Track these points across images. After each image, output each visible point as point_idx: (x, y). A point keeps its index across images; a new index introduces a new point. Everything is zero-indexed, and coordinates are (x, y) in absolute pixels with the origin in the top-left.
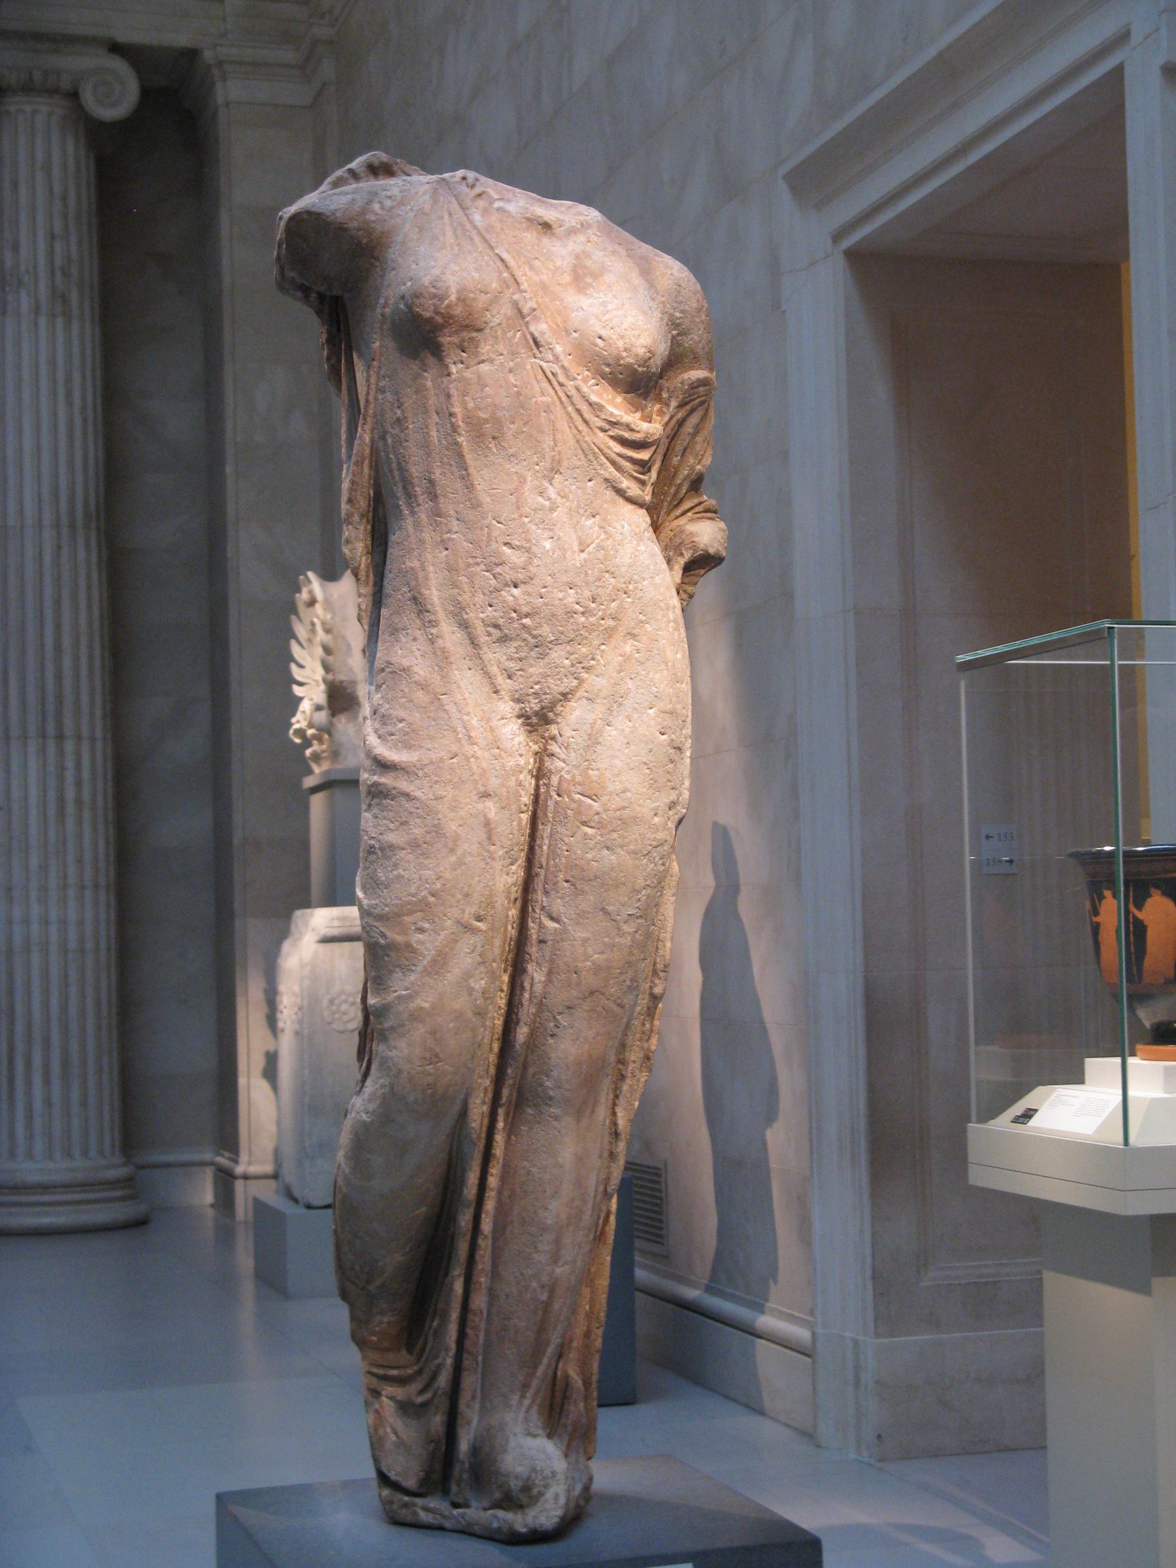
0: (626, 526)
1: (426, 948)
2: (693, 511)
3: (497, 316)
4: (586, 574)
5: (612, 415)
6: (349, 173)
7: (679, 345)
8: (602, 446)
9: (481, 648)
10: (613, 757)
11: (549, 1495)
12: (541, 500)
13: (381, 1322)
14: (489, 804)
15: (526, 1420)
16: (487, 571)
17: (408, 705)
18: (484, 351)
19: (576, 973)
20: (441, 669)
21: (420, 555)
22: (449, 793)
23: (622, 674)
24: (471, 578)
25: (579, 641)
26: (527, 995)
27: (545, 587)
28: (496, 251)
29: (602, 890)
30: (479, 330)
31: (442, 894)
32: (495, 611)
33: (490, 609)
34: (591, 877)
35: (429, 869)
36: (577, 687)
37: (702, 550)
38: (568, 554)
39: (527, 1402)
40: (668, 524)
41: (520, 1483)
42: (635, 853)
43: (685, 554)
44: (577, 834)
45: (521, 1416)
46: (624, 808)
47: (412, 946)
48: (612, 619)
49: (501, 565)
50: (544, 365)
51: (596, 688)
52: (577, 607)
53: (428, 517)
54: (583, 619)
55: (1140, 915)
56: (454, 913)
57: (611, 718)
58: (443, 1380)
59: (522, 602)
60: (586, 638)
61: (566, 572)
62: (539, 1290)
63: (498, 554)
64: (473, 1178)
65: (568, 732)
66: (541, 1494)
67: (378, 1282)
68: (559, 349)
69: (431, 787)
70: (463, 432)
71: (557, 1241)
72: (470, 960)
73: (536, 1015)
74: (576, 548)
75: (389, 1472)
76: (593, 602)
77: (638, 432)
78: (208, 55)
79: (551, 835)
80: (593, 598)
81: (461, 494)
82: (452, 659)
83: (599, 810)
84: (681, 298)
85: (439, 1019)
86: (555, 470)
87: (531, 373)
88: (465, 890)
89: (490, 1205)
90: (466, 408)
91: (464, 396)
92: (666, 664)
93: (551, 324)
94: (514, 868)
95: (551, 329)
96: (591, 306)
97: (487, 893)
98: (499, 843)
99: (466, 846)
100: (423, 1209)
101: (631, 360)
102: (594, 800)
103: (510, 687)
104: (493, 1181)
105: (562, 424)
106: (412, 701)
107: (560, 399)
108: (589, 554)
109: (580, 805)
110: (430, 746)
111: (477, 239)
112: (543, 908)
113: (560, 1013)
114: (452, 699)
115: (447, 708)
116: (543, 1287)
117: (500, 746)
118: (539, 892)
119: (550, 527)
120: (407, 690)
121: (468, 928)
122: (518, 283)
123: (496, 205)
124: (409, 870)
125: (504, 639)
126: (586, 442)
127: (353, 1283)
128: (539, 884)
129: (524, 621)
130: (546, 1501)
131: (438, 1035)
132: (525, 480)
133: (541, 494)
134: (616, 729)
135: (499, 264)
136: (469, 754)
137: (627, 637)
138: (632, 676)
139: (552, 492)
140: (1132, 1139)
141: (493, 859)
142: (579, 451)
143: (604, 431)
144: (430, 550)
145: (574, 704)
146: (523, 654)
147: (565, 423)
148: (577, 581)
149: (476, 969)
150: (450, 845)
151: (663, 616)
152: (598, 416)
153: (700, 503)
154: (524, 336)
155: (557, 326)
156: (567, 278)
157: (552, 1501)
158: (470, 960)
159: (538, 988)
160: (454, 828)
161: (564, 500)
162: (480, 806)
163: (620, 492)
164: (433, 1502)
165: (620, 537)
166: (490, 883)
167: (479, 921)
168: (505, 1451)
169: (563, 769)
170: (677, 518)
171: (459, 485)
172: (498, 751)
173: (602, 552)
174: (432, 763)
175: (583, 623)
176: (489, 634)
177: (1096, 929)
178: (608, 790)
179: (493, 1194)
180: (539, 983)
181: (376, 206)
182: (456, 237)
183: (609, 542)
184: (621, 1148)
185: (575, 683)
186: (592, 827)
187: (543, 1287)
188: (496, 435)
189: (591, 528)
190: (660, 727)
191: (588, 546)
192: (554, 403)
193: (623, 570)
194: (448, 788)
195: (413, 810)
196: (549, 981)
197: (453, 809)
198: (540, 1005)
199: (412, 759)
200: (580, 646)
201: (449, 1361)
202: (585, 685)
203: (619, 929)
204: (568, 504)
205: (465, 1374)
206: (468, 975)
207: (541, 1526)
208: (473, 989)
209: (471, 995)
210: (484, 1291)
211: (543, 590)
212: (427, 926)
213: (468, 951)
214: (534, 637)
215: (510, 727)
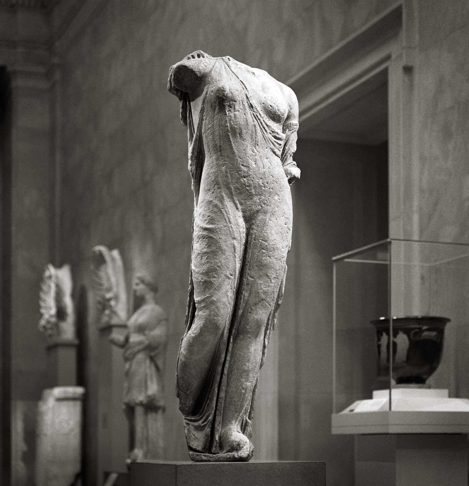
1: (216, 282)
5: (273, 129)
6: (192, 56)
8: (270, 138)
10: (271, 229)
11: (245, 448)
14: (235, 241)
15: (237, 428)
19: (258, 293)
26: (242, 300)
30: (235, 101)
31: (221, 267)
33: (237, 184)
35: (217, 259)
37: (293, 175)
46: (274, 245)
47: (211, 281)
52: (262, 185)
55: (396, 340)
58: (211, 418)
59: (246, 182)
60: (264, 194)
64: (223, 356)
70: (230, 132)
73: (245, 306)
75: (193, 446)
78: (10, 69)
79: (252, 252)
80: (267, 182)
86: (256, 144)
89: (227, 365)
102: (265, 242)
104: (228, 358)
112: (248, 274)
113: (252, 306)
115: (223, 212)
117: (239, 225)
118: (247, 270)
119: (255, 161)
125: (240, 193)
126: (266, 137)
127: (182, 391)
128: (247, 267)
129: (247, 188)
130: (244, 449)
131: (218, 309)
136: (230, 226)
140: (393, 409)
143: (270, 133)
145: (260, 214)
146: (246, 198)
148: (262, 177)
152: (269, 129)
156: (260, 89)
159: (246, 298)
162: (232, 241)
167: (231, 276)
169: (256, 233)
171: (228, 147)
172: (238, 226)
175: (264, 189)
176: (236, 191)
177: (379, 346)
178: (270, 239)
179: (228, 362)
183: (271, 167)
184: (266, 351)
186: (265, 250)
188: (240, 133)
191: (266, 167)
193: (276, 175)
196: (249, 296)
197: (225, 242)
198: (246, 303)
201: (213, 412)
205: (217, 417)
210: (224, 392)
211: (253, 179)
212: (216, 276)
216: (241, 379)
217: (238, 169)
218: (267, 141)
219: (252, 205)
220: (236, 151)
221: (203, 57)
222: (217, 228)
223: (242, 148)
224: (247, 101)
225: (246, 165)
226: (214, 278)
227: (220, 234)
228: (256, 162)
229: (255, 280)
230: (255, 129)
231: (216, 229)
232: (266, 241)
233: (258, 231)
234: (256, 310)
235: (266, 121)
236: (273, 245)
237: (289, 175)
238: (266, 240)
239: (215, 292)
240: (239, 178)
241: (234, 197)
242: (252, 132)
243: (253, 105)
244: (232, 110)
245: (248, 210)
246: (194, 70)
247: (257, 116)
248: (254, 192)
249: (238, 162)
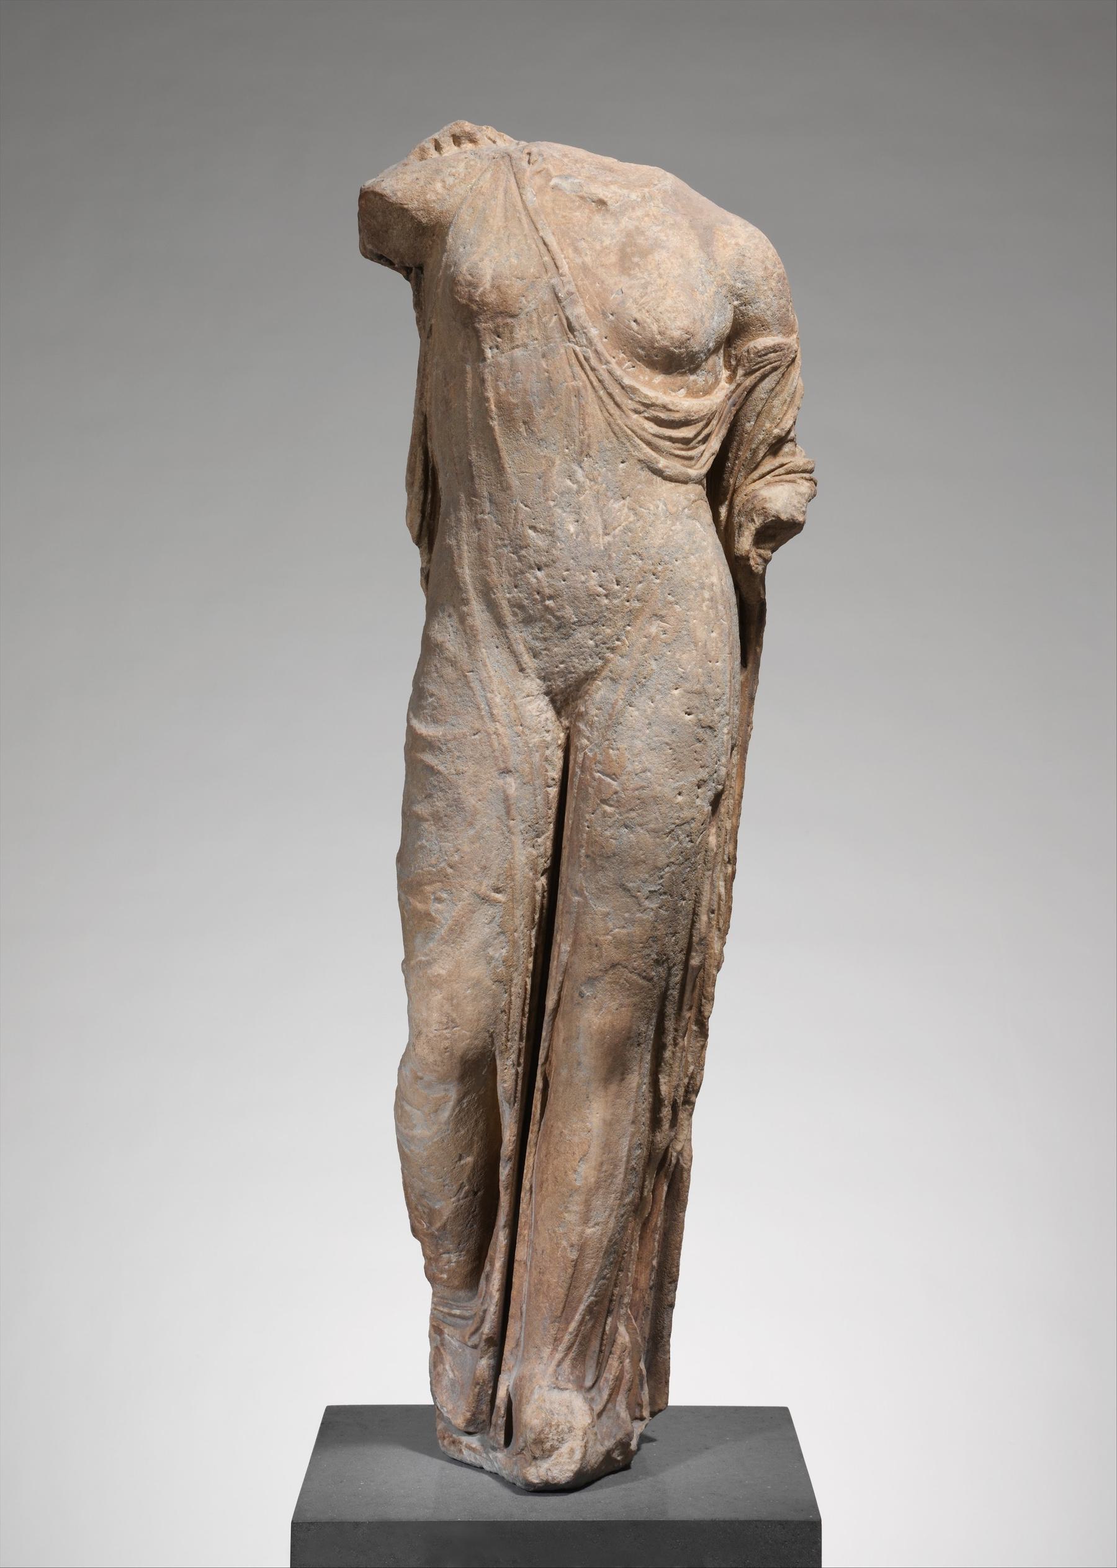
0: (661, 505)
1: (444, 918)
2: (773, 474)
3: (534, 302)
5: (646, 396)
8: (636, 428)
9: (507, 628)
10: (633, 737)
11: (565, 1449)
12: (569, 482)
13: (449, 1262)
15: (556, 1374)
16: (513, 553)
18: (518, 336)
20: (469, 646)
21: (457, 533)
22: (470, 769)
23: (646, 655)
24: (498, 558)
27: (568, 570)
28: (541, 234)
29: (621, 867)
30: (513, 316)
32: (520, 592)
34: (610, 854)
35: (448, 842)
36: (602, 667)
37: (773, 516)
38: (592, 538)
39: (558, 1356)
40: (744, 488)
41: (533, 1436)
43: (756, 519)
44: (597, 811)
45: (551, 1369)
46: (643, 788)
47: (430, 914)
48: (638, 600)
49: (526, 547)
50: (578, 349)
52: (600, 589)
54: (606, 601)
57: (633, 699)
59: (545, 584)
60: (610, 619)
61: (589, 555)
62: (569, 1249)
63: (522, 536)
65: (594, 712)
66: (554, 1449)
68: (594, 332)
69: (453, 762)
71: (587, 1203)
72: (487, 930)
80: (617, 581)
82: (480, 637)
83: (618, 789)
84: (744, 269)
85: (456, 986)
86: (584, 452)
87: (564, 357)
90: (498, 393)
91: (497, 381)
92: (696, 644)
93: (588, 306)
94: (539, 840)
95: (588, 312)
96: (630, 287)
97: (506, 866)
100: (469, 1160)
101: (666, 343)
102: (613, 779)
103: (536, 665)
105: (593, 408)
106: (442, 676)
107: (591, 383)
108: (614, 537)
110: (454, 722)
116: (572, 1246)
119: (577, 511)
120: (439, 665)
121: (485, 900)
122: (557, 267)
124: (431, 841)
125: (528, 621)
126: (618, 425)
129: (547, 602)
131: (455, 1001)
132: (554, 463)
133: (570, 477)
134: (638, 710)
135: (542, 247)
136: (492, 730)
138: (657, 657)
139: (580, 474)
141: (512, 833)
142: (612, 434)
143: (636, 411)
144: (465, 529)
145: (600, 683)
147: (597, 407)
148: (600, 564)
149: (495, 938)
150: (469, 819)
152: (631, 399)
153: (782, 465)
154: (560, 319)
155: (595, 308)
156: (613, 258)
157: (566, 1456)
158: (487, 930)
160: (474, 802)
161: (592, 483)
162: (501, 782)
163: (658, 472)
164: (474, 1441)
165: (653, 518)
166: (510, 857)
169: (587, 746)
170: (755, 481)
172: (521, 728)
173: (630, 534)
174: (455, 738)
175: (606, 605)
178: (627, 769)
180: (565, 952)
182: (506, 218)
185: (600, 663)
186: (611, 806)
187: (572, 1246)
188: (526, 419)
189: (619, 510)
190: (686, 707)
191: (614, 529)
192: (585, 387)
193: (652, 551)
195: (436, 783)
196: (573, 951)
197: (475, 784)
198: (565, 972)
200: (604, 627)
202: (610, 665)
203: (640, 905)
204: (596, 487)
206: (486, 944)
207: (553, 1478)
208: (492, 958)
211: (565, 573)
212: (444, 896)
213: (486, 921)
214: (557, 618)
215: (536, 704)
216: (566, 1215)
217: (519, 542)
219: (570, 656)
220: (515, 482)
221: (473, 141)
222: (449, 737)
223: (532, 470)
224: (558, 310)
225: (542, 526)
227: (459, 757)
228: (578, 514)
230: (580, 403)
231: (449, 741)
232: (613, 776)
233: (591, 743)
234: (595, 998)
236: (637, 790)
237: (758, 515)
238: (614, 774)
240: (522, 572)
241: (508, 631)
242: (569, 414)
243: (575, 324)
245: (558, 672)
247: (587, 359)
249: (520, 517)
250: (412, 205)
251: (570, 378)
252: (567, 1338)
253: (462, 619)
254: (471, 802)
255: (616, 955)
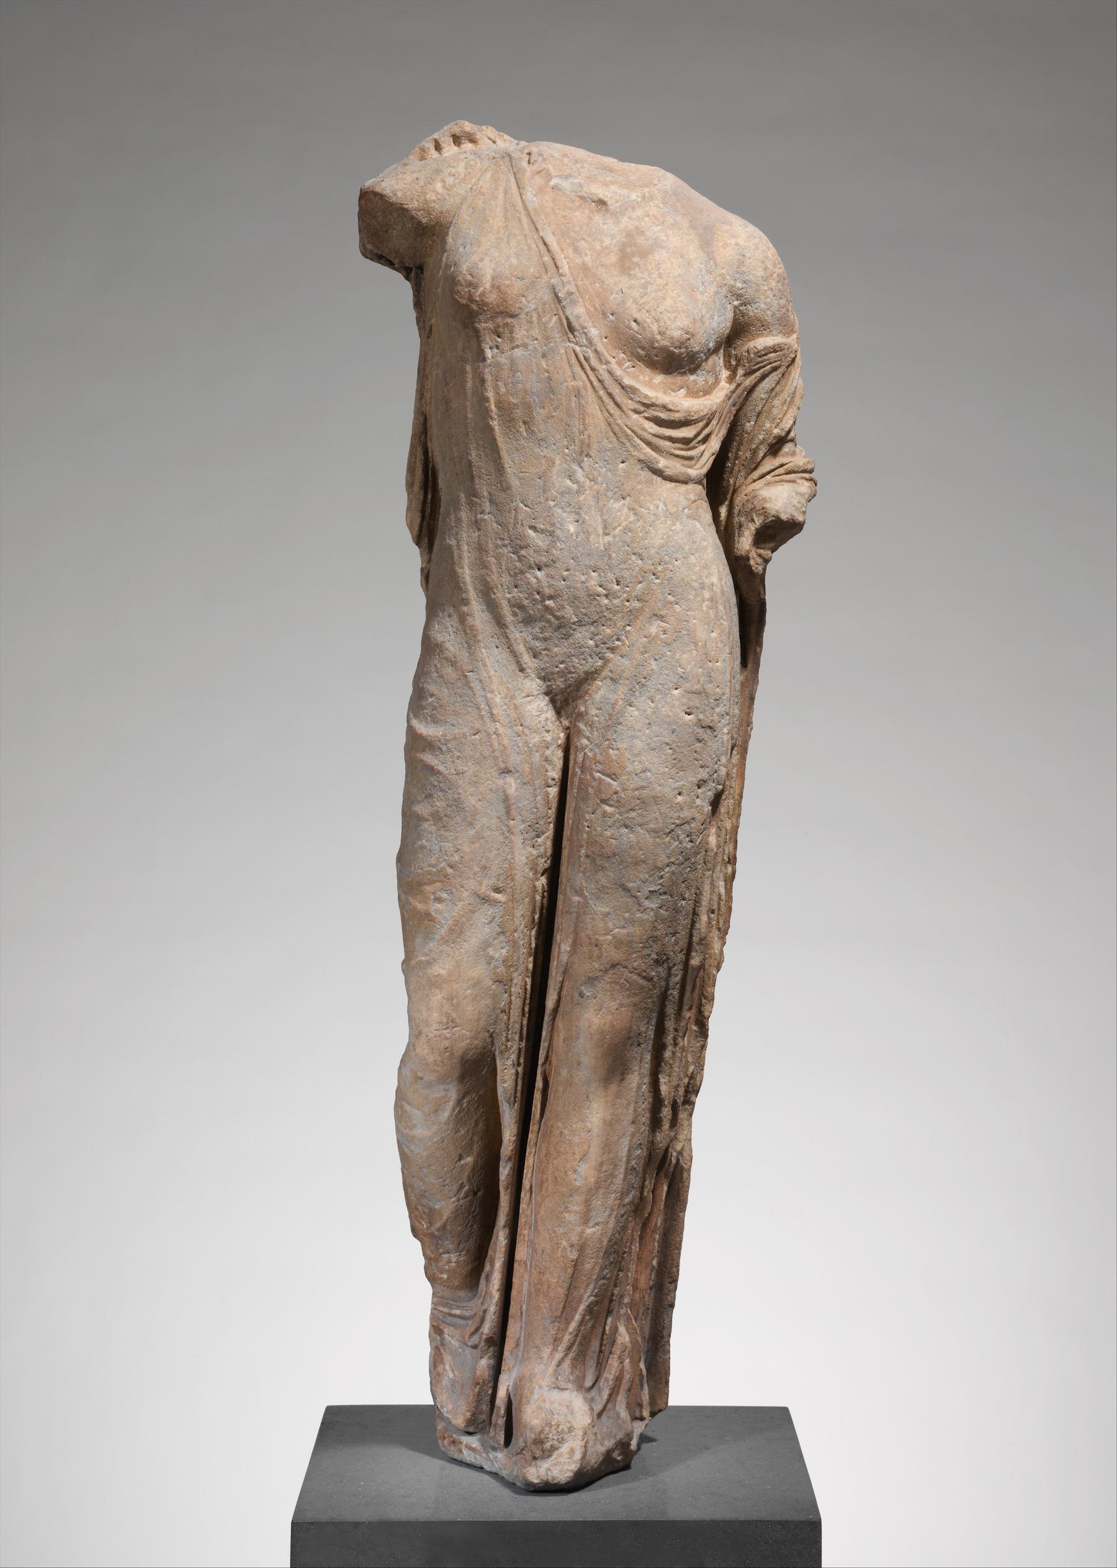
0: (661, 505)
1: (444, 918)
2: (773, 474)
4: (610, 557)
5: (646, 396)
7: (743, 315)
8: (635, 428)
9: (507, 628)
10: (633, 737)
11: (565, 1449)
12: (568, 482)
13: (449, 1262)
17: (439, 680)
18: (518, 336)
20: (469, 647)
21: (457, 533)
22: (470, 768)
23: (646, 655)
24: (498, 558)
25: (603, 622)
28: (541, 234)
29: (621, 867)
30: (513, 316)
31: (460, 866)
34: (610, 854)
35: (448, 842)
36: (602, 667)
37: (773, 516)
38: (592, 537)
39: (558, 1356)
41: (533, 1436)
42: (654, 831)
43: (756, 519)
44: (597, 811)
45: (551, 1369)
46: (643, 788)
47: (430, 914)
48: (638, 600)
49: (526, 547)
50: (578, 349)
51: (620, 668)
52: (600, 589)
53: (466, 497)
54: (606, 601)
56: (472, 884)
59: (545, 584)
60: (610, 619)
61: (589, 555)
62: (569, 1249)
65: (593, 712)
66: (554, 1448)
67: (438, 1224)
68: (594, 332)
74: (601, 531)
76: (618, 585)
77: (678, 411)
81: (494, 476)
82: (480, 637)
83: (618, 789)
84: (744, 269)
86: (584, 452)
87: (564, 357)
88: (482, 863)
90: (498, 393)
91: (497, 381)
92: (696, 644)
94: (539, 840)
95: (588, 312)
97: (506, 866)
98: (520, 817)
99: (485, 820)
100: (469, 1160)
101: (666, 343)
102: (613, 780)
103: (536, 665)
105: (593, 408)
106: (442, 677)
107: (591, 383)
108: (614, 536)
109: (600, 783)
110: (454, 722)
111: (525, 220)
114: (477, 677)
115: (472, 685)
116: (572, 1246)
120: (439, 666)
121: (485, 900)
122: (557, 267)
123: (553, 182)
124: (431, 841)
125: (528, 621)
126: (618, 425)
129: (547, 602)
131: (455, 1001)
132: (553, 463)
133: (570, 477)
134: (638, 710)
136: (492, 730)
137: (653, 619)
138: (657, 657)
139: (580, 474)
141: (512, 833)
142: (611, 434)
143: (636, 412)
145: (600, 683)
147: (597, 407)
148: (600, 564)
149: (495, 939)
150: (469, 819)
151: (696, 595)
152: (632, 399)
153: (782, 465)
154: (560, 320)
155: (595, 309)
156: (613, 258)
157: (566, 1456)
161: (592, 483)
162: (500, 782)
163: (658, 472)
164: (474, 1441)
165: (653, 518)
166: (510, 857)
168: (528, 1402)
169: (587, 746)
170: (754, 481)
172: (521, 728)
173: (630, 534)
174: (455, 738)
175: (606, 605)
178: (627, 769)
181: (439, 186)
182: (506, 218)
185: (600, 663)
186: (611, 806)
187: (572, 1246)
188: (526, 419)
189: (619, 510)
190: (686, 707)
191: (614, 529)
192: (585, 387)
193: (652, 551)
194: (470, 763)
195: (436, 783)
196: (573, 951)
197: (475, 784)
198: (565, 972)
199: (436, 734)
200: (604, 627)
202: (610, 665)
204: (596, 487)
206: (486, 945)
207: (553, 1478)
209: (489, 963)
211: (565, 573)
212: (445, 896)
213: (486, 921)
214: (557, 618)
215: (536, 704)
216: (566, 1215)
217: (519, 542)
218: (623, 440)
219: (570, 656)
220: (515, 482)
221: (473, 141)
222: (449, 737)
223: (533, 470)
225: (542, 526)
226: (439, 903)
227: (458, 757)
228: (578, 514)
229: (586, 904)
230: (579, 403)
231: (449, 741)
232: (613, 776)
235: (618, 372)
236: (637, 790)
237: (759, 515)
238: (614, 774)
239: (441, 948)
240: (522, 572)
241: (508, 631)
242: (570, 415)
244: (506, 346)
245: (558, 672)
246: (406, 206)
247: (586, 359)
248: (573, 616)
249: (520, 517)
250: (412, 205)
251: (570, 378)
252: (567, 1338)
253: (462, 619)
254: (471, 802)
255: (616, 955)
